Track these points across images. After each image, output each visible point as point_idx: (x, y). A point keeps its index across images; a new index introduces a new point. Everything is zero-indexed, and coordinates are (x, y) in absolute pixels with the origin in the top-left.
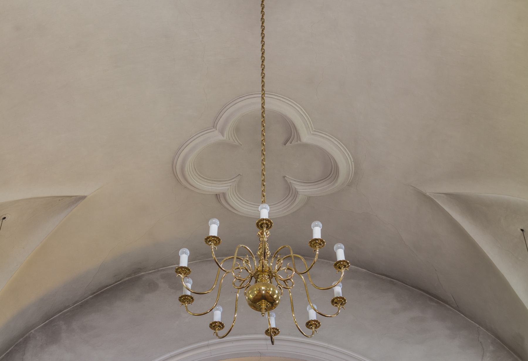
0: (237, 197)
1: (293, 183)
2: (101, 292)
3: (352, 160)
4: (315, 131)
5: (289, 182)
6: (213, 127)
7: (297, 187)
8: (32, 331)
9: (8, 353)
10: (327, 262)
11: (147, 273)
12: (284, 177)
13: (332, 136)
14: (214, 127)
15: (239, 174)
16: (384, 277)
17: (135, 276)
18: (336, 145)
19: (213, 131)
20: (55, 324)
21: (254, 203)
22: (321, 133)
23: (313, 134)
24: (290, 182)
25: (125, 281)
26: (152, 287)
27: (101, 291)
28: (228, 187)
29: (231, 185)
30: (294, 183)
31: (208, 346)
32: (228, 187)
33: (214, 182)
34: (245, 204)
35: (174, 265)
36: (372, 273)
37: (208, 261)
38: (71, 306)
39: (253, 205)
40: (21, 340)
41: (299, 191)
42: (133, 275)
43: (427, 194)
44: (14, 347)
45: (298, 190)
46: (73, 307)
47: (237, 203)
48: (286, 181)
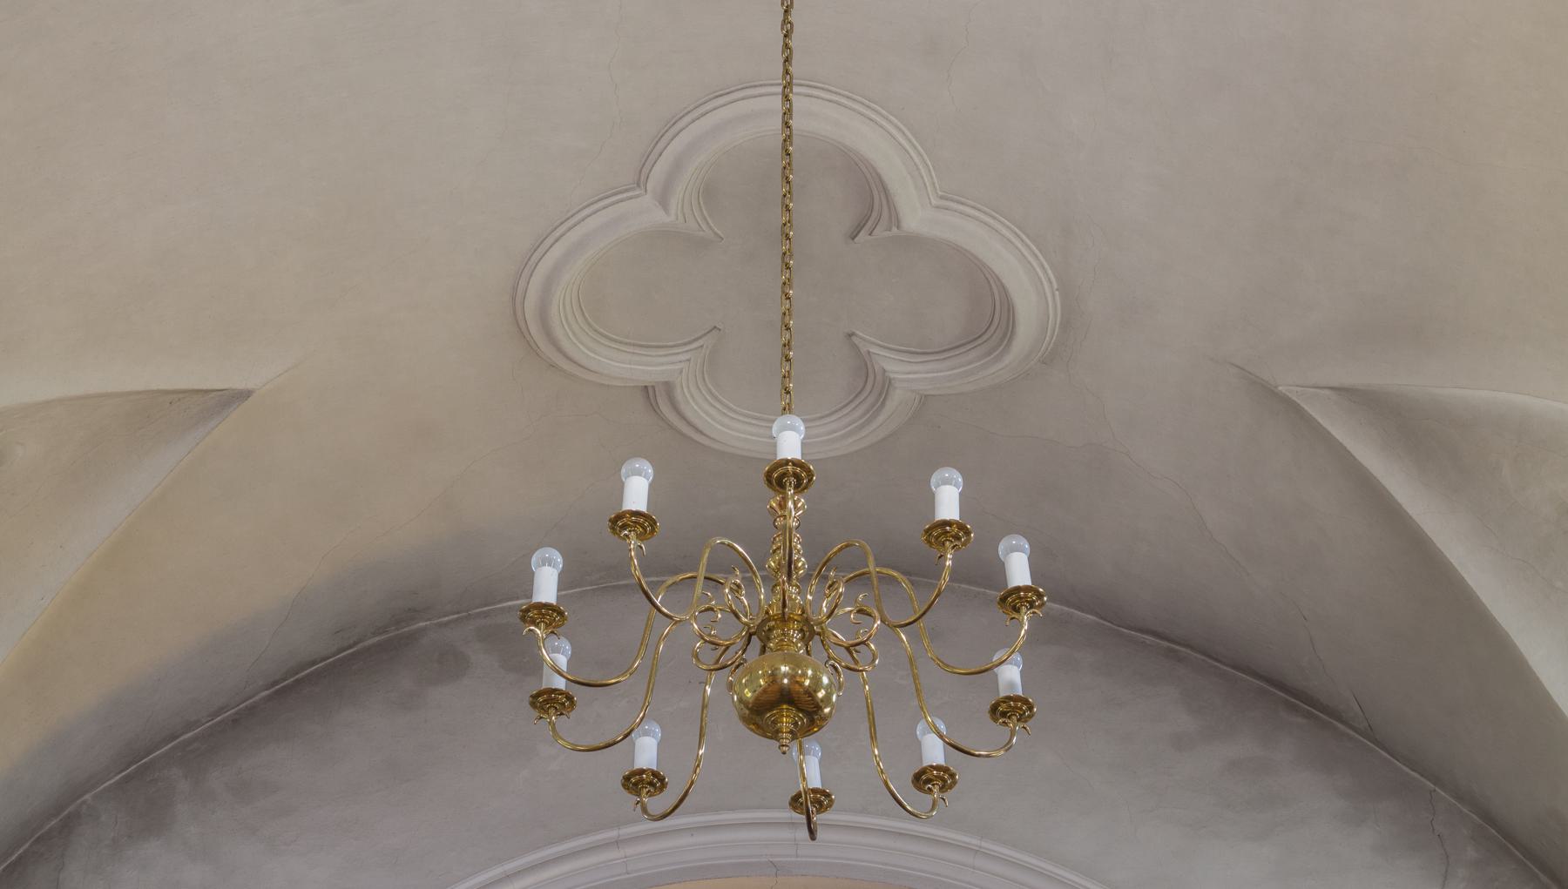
3: (1055, 286)
4: (942, 198)
5: (863, 350)
7: (888, 367)
8: (87, 797)
10: (979, 593)
13: (994, 213)
16: (1149, 639)
17: (397, 632)
19: (637, 196)
23: (937, 207)
29: (689, 360)
32: (678, 367)
33: (637, 350)
38: (204, 721)
41: (894, 379)
44: (31, 846)
45: (892, 376)
48: (855, 347)
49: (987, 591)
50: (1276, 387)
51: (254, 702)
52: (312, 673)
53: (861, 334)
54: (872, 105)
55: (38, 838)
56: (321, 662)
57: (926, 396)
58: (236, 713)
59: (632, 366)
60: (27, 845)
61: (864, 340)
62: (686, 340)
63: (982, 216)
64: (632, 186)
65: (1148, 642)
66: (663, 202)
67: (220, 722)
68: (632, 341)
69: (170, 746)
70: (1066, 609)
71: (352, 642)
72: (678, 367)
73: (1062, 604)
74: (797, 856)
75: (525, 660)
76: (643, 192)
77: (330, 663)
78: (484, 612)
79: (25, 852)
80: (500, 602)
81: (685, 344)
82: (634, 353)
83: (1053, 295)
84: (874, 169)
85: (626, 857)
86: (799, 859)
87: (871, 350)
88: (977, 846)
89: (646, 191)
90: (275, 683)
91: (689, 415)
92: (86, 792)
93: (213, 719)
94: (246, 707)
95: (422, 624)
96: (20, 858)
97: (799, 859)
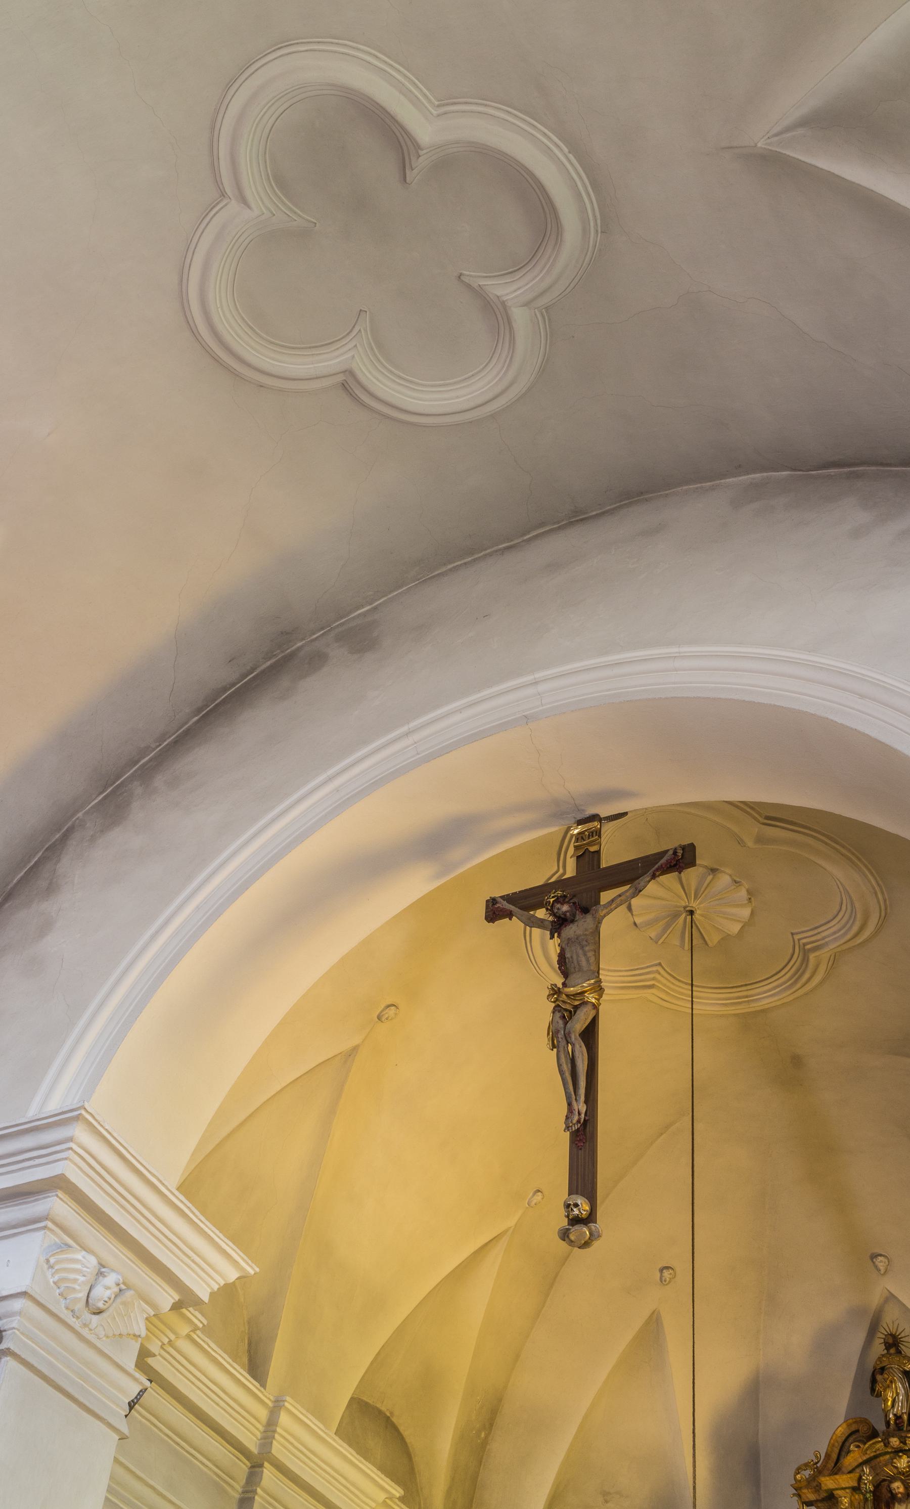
0: (393, 378)
1: (485, 285)
2: (216, 705)
3: (566, 150)
4: (439, 106)
5: (475, 285)
6: (222, 197)
7: (499, 292)
8: (80, 815)
9: (32, 868)
10: (697, 488)
11: (308, 641)
12: (460, 277)
13: (485, 102)
14: (224, 196)
15: (361, 310)
16: (832, 471)
17: (283, 654)
18: (503, 119)
19: (226, 205)
20: (123, 790)
21: (443, 382)
22: (455, 104)
23: (438, 116)
24: (479, 285)
25: (263, 672)
26: (317, 661)
27: (216, 702)
28: (353, 353)
29: (356, 346)
30: (487, 285)
31: (407, 734)
32: (350, 355)
33: (315, 351)
34: (394, 381)
35: (363, 607)
36: (805, 473)
37: (434, 577)
38: (153, 746)
39: (440, 386)
40: (57, 836)
41: (506, 300)
42: (279, 651)
43: (759, 145)
44: (43, 854)
45: (505, 299)
46: (160, 750)
47: (420, 400)
48: (469, 286)
49: (703, 484)
50: (756, 146)
51: (189, 727)
52: (226, 697)
53: (468, 273)
54: (340, 41)
55: (47, 849)
56: (230, 688)
57: (547, 309)
58: (177, 737)
59: (316, 365)
60: (40, 854)
61: (471, 276)
62: (348, 331)
63: (474, 108)
64: (220, 199)
65: (832, 474)
66: (244, 201)
67: (167, 745)
68: (308, 346)
69: (134, 769)
70: (765, 474)
71: (248, 668)
72: (350, 355)
73: (761, 472)
74: (542, 705)
75: (365, 643)
76: (229, 200)
77: (238, 688)
78: (341, 623)
79: (39, 859)
80: (350, 612)
81: (348, 334)
82: (313, 355)
83: (569, 161)
84: (369, 97)
85: (415, 743)
86: (544, 707)
87: (480, 284)
88: (677, 653)
89: (230, 198)
90: (199, 710)
91: (379, 394)
92: (77, 811)
93: (160, 745)
94: (184, 731)
95: (299, 644)
96: (36, 863)
97: (544, 707)
